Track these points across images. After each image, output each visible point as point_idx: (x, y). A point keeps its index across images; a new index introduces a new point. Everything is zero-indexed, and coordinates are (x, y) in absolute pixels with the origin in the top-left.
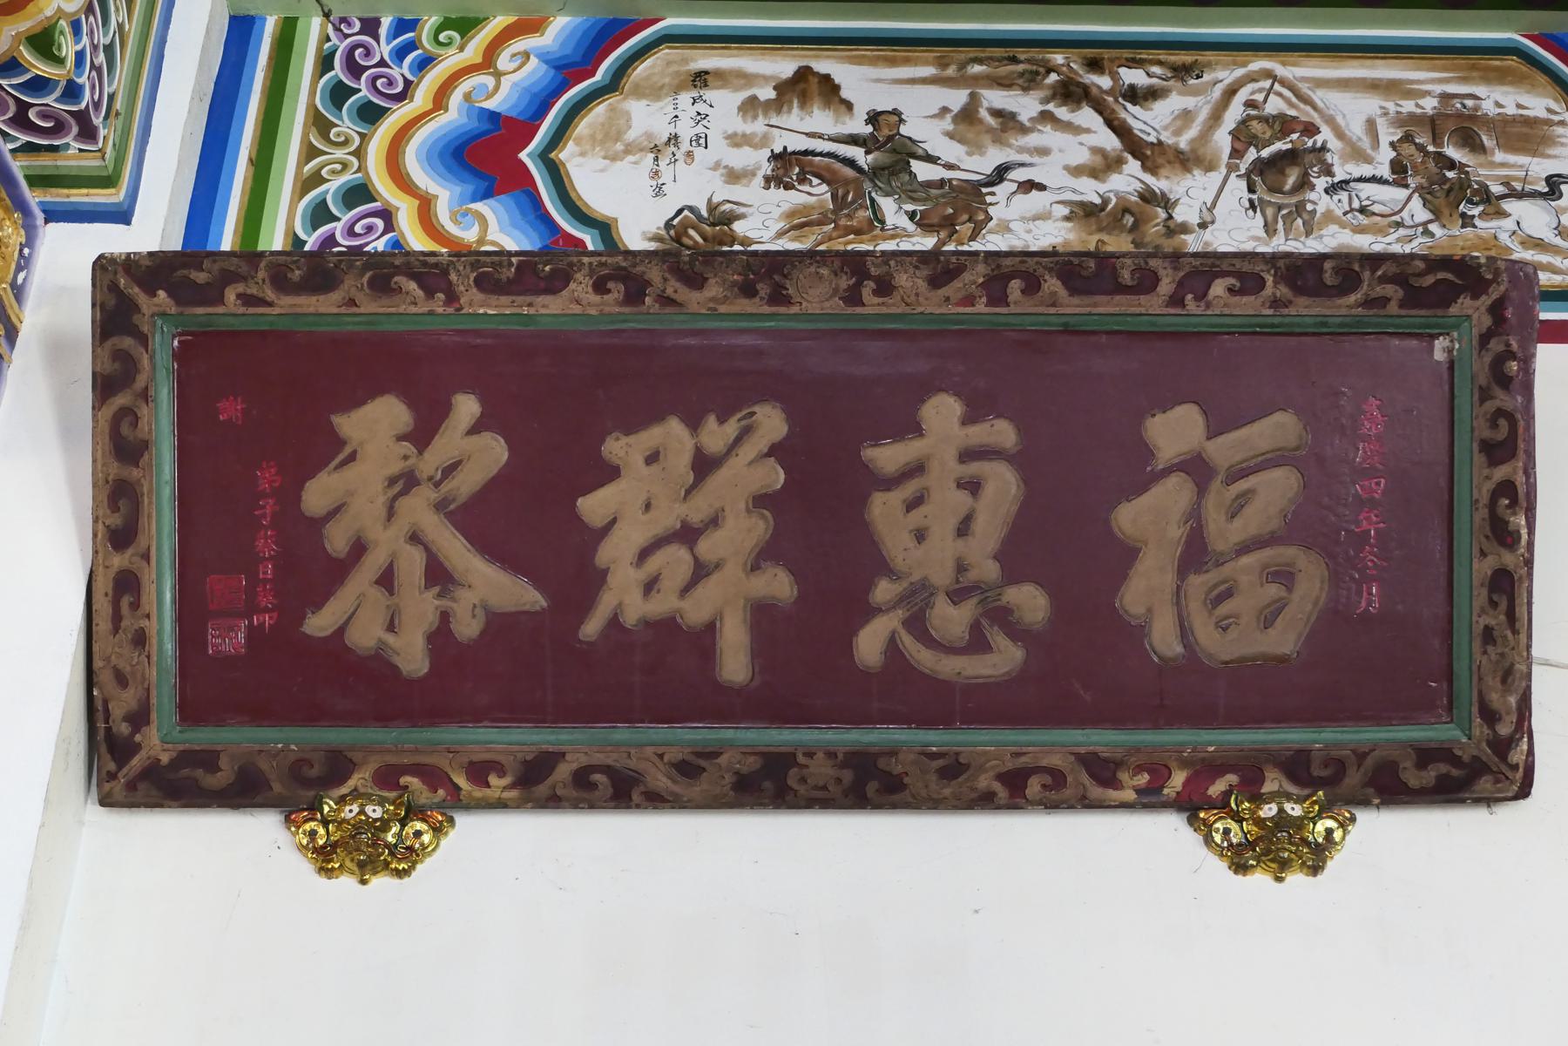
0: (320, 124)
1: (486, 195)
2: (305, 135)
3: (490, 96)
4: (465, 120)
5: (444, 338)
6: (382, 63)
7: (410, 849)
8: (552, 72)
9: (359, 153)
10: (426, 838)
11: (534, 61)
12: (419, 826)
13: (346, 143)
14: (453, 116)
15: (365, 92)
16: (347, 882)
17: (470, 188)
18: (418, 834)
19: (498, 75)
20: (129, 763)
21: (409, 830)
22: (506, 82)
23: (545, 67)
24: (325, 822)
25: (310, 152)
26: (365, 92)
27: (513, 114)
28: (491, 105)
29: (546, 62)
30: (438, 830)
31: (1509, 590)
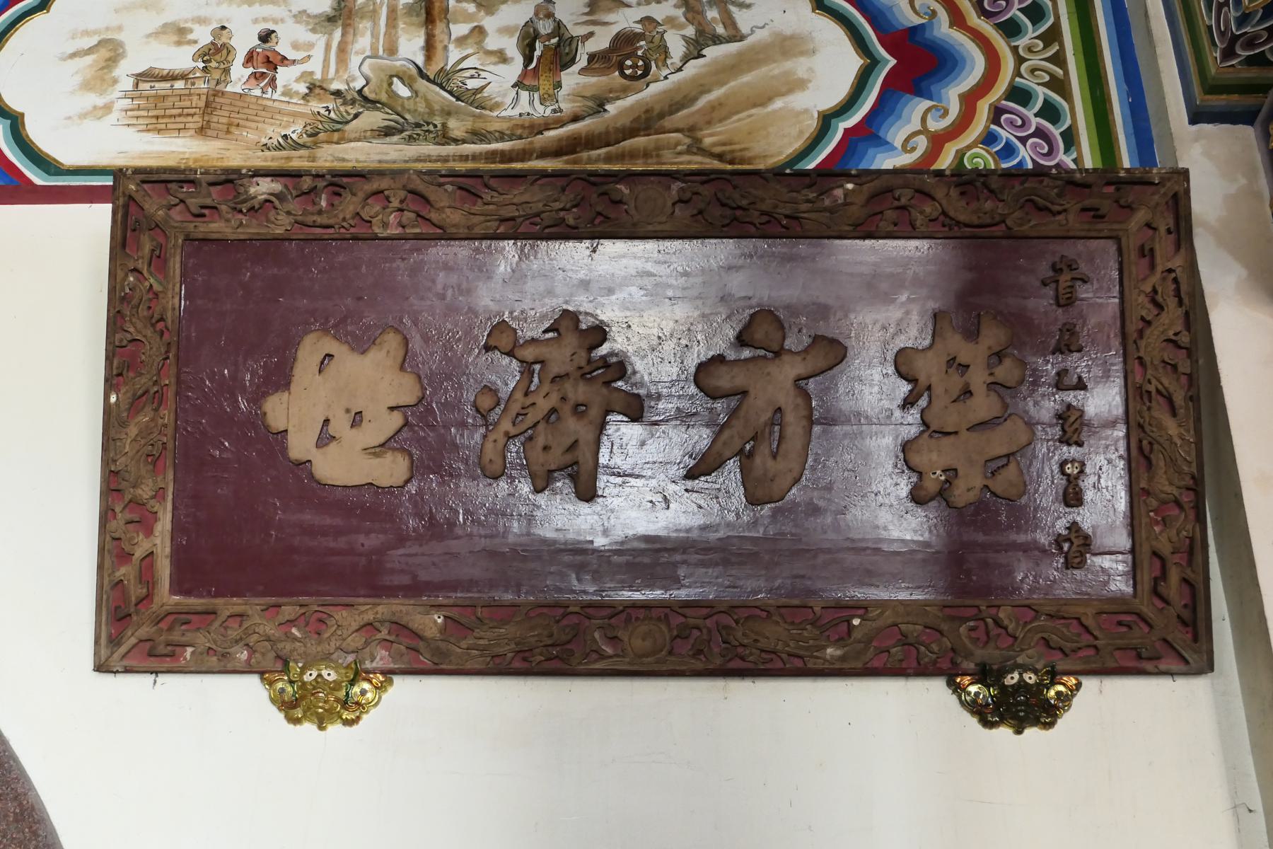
0: (1060, 86)
1: (914, 30)
2: (1066, 73)
3: (928, 110)
4: (933, 88)
5: (516, 192)
6: (1023, 140)
7: (357, 703)
8: (881, 134)
9: (1020, 60)
10: (369, 696)
11: (898, 143)
12: (366, 686)
13: (1033, 71)
14: (952, 95)
15: (1029, 113)
16: (309, 728)
17: (927, 35)
18: (363, 692)
19: (924, 130)
20: (136, 631)
21: (356, 689)
22: (915, 125)
23: (889, 139)
24: (291, 682)
25: (1059, 59)
26: (1029, 113)
27: (918, 99)
28: (927, 104)
29: (887, 143)
30: (380, 688)
31: (1234, 460)
